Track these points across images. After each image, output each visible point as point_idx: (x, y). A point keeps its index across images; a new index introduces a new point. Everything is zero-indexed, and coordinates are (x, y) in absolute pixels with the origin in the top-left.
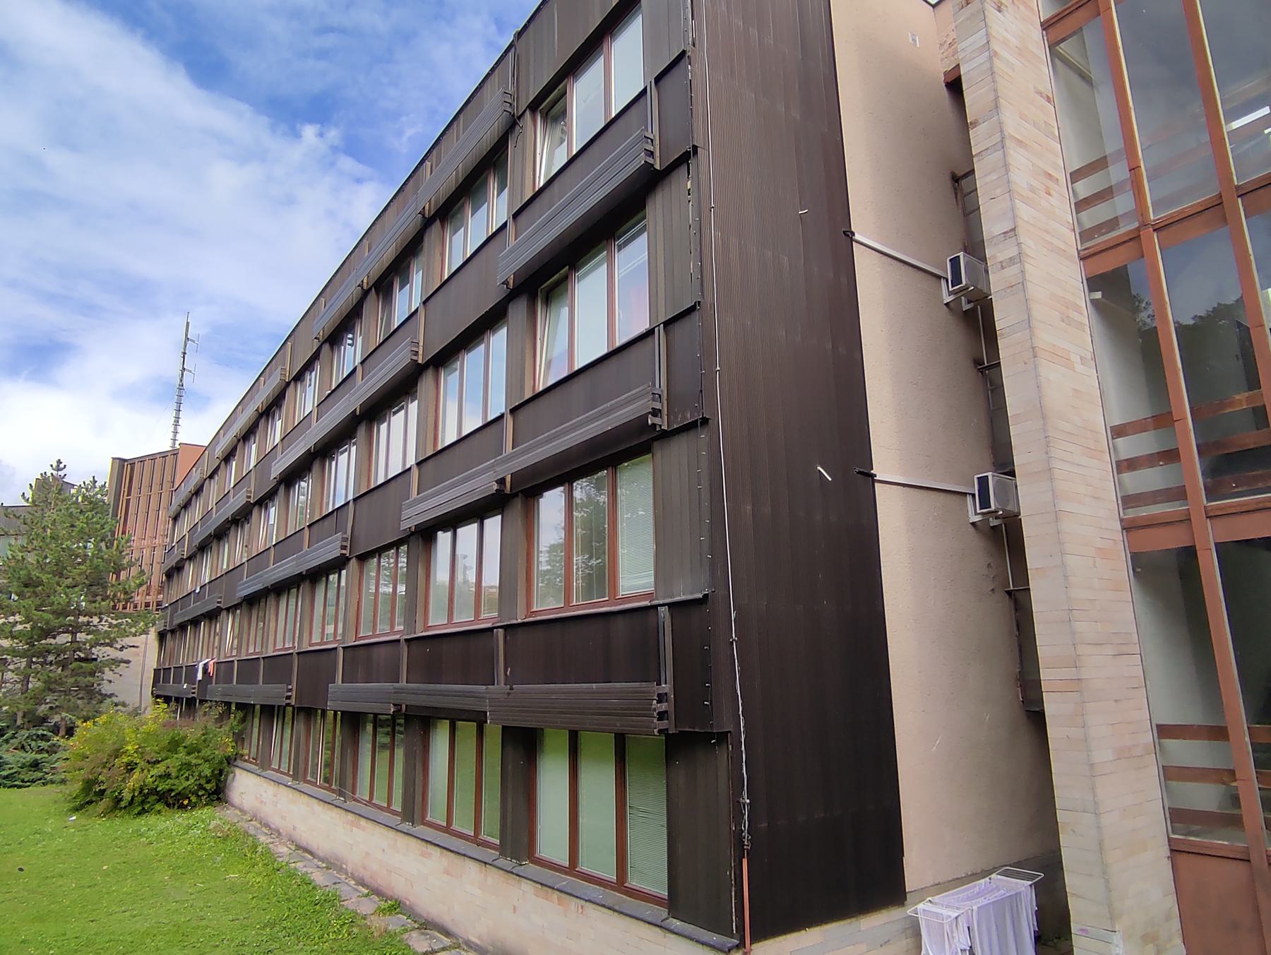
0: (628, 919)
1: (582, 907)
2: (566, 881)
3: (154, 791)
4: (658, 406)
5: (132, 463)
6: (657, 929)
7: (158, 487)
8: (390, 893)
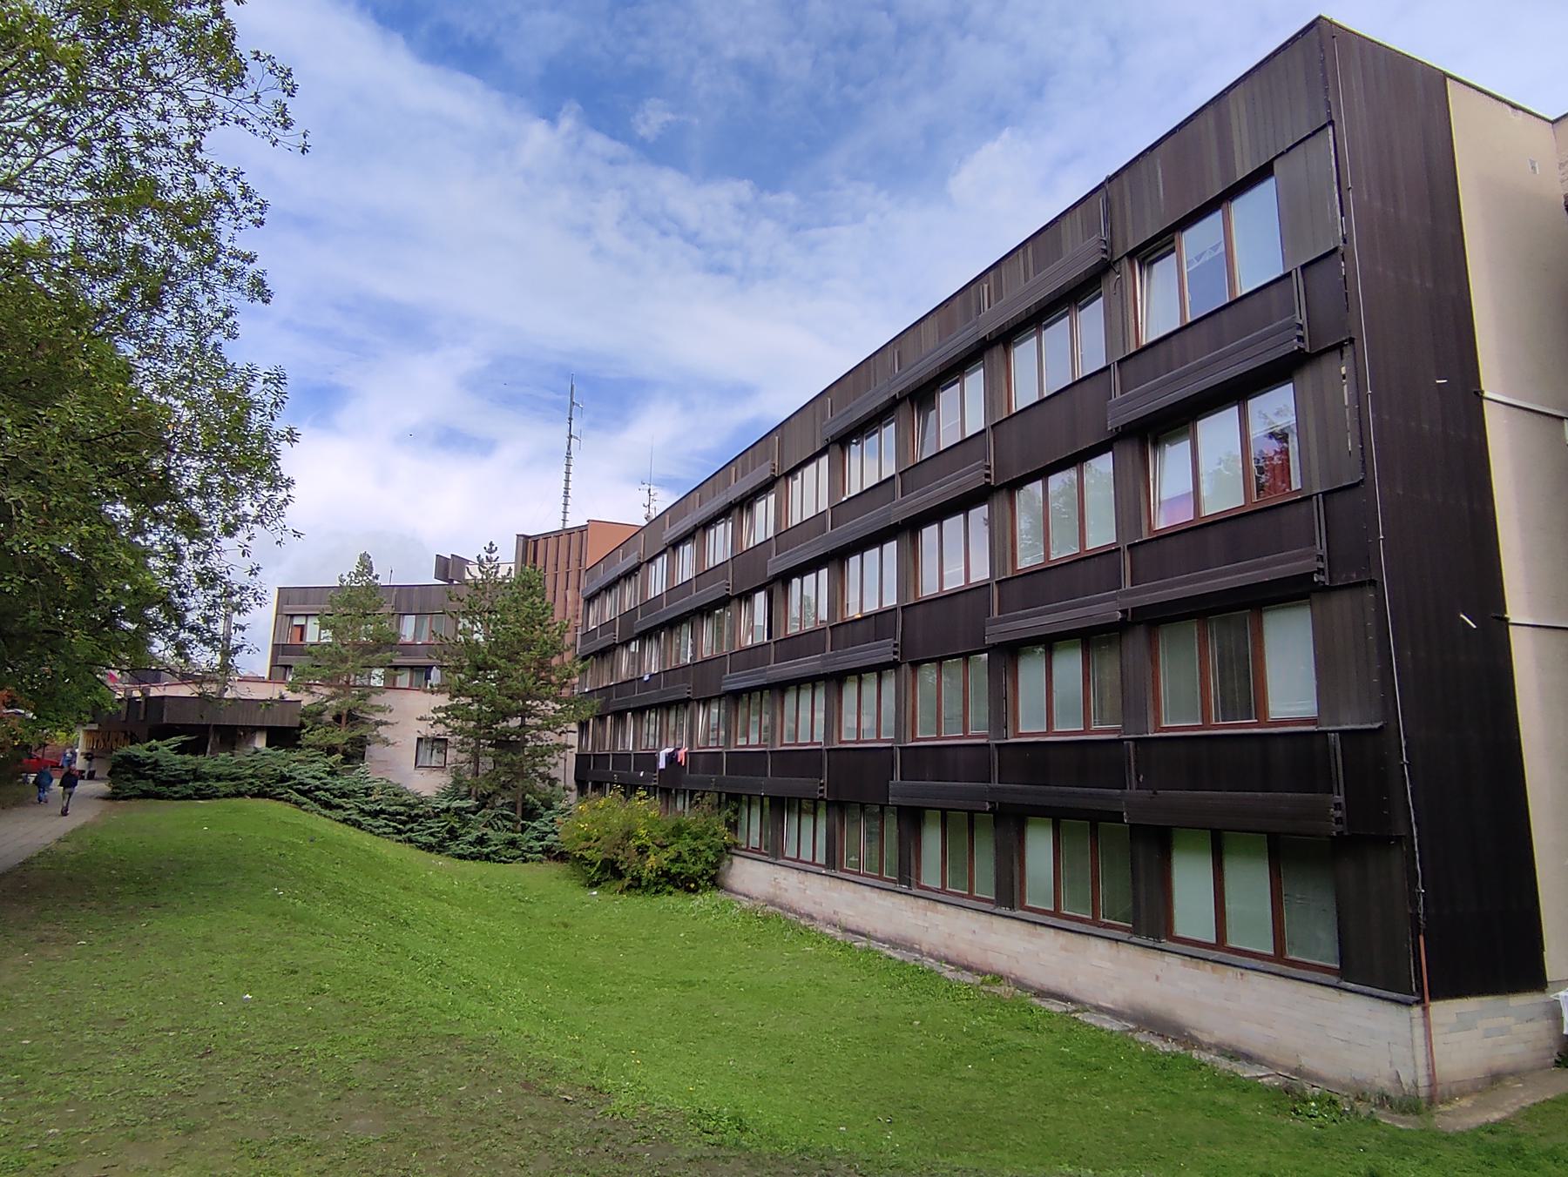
0: (1297, 983)
1: (1242, 974)
2: (1217, 955)
3: (666, 873)
4: (1321, 565)
6: (1331, 990)
7: (553, 568)
8: (987, 969)
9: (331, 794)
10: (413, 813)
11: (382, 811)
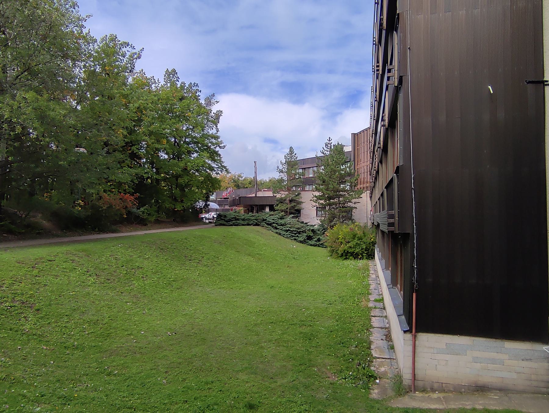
5: (357, 134)
9: (278, 225)
10: (299, 231)
11: (289, 230)
